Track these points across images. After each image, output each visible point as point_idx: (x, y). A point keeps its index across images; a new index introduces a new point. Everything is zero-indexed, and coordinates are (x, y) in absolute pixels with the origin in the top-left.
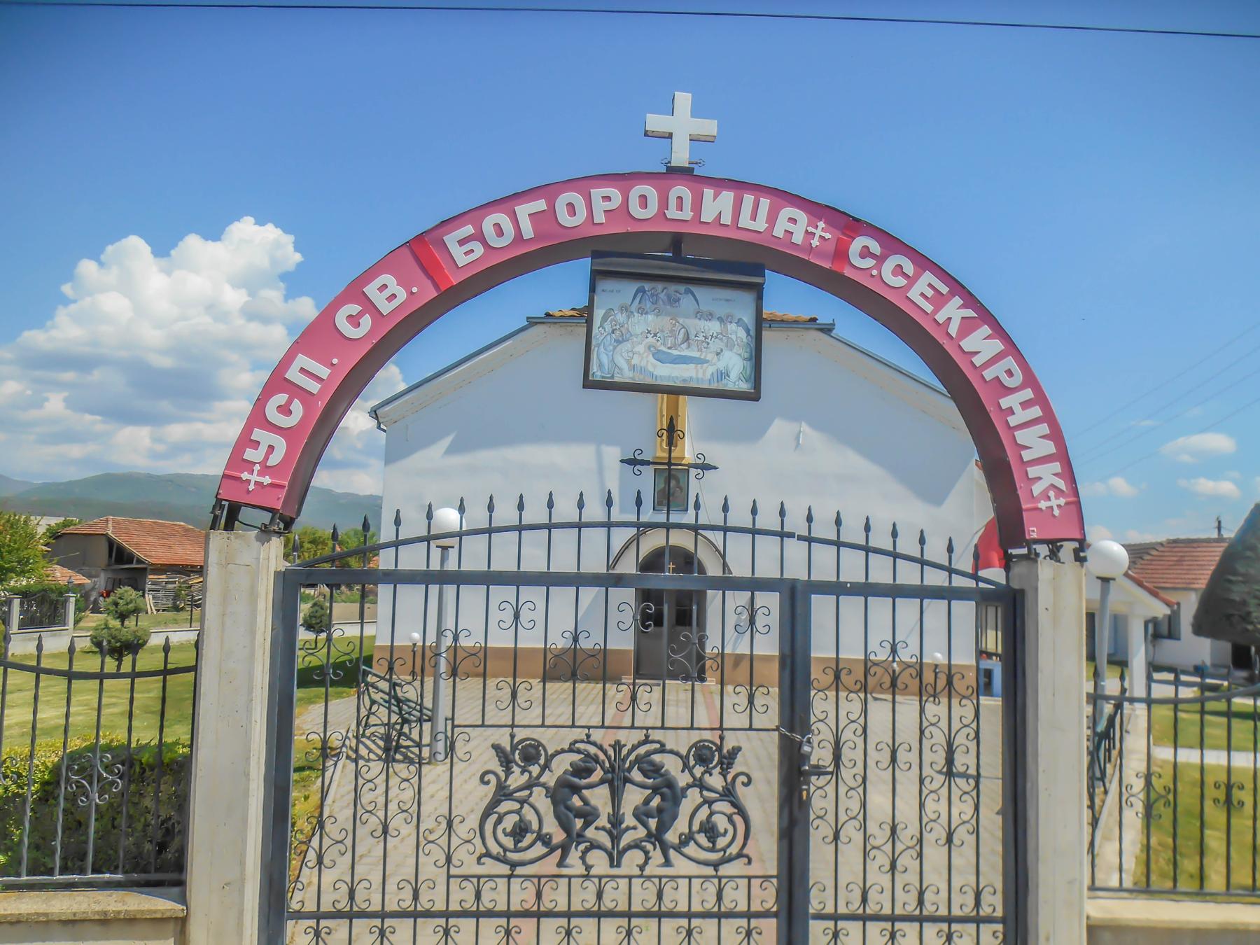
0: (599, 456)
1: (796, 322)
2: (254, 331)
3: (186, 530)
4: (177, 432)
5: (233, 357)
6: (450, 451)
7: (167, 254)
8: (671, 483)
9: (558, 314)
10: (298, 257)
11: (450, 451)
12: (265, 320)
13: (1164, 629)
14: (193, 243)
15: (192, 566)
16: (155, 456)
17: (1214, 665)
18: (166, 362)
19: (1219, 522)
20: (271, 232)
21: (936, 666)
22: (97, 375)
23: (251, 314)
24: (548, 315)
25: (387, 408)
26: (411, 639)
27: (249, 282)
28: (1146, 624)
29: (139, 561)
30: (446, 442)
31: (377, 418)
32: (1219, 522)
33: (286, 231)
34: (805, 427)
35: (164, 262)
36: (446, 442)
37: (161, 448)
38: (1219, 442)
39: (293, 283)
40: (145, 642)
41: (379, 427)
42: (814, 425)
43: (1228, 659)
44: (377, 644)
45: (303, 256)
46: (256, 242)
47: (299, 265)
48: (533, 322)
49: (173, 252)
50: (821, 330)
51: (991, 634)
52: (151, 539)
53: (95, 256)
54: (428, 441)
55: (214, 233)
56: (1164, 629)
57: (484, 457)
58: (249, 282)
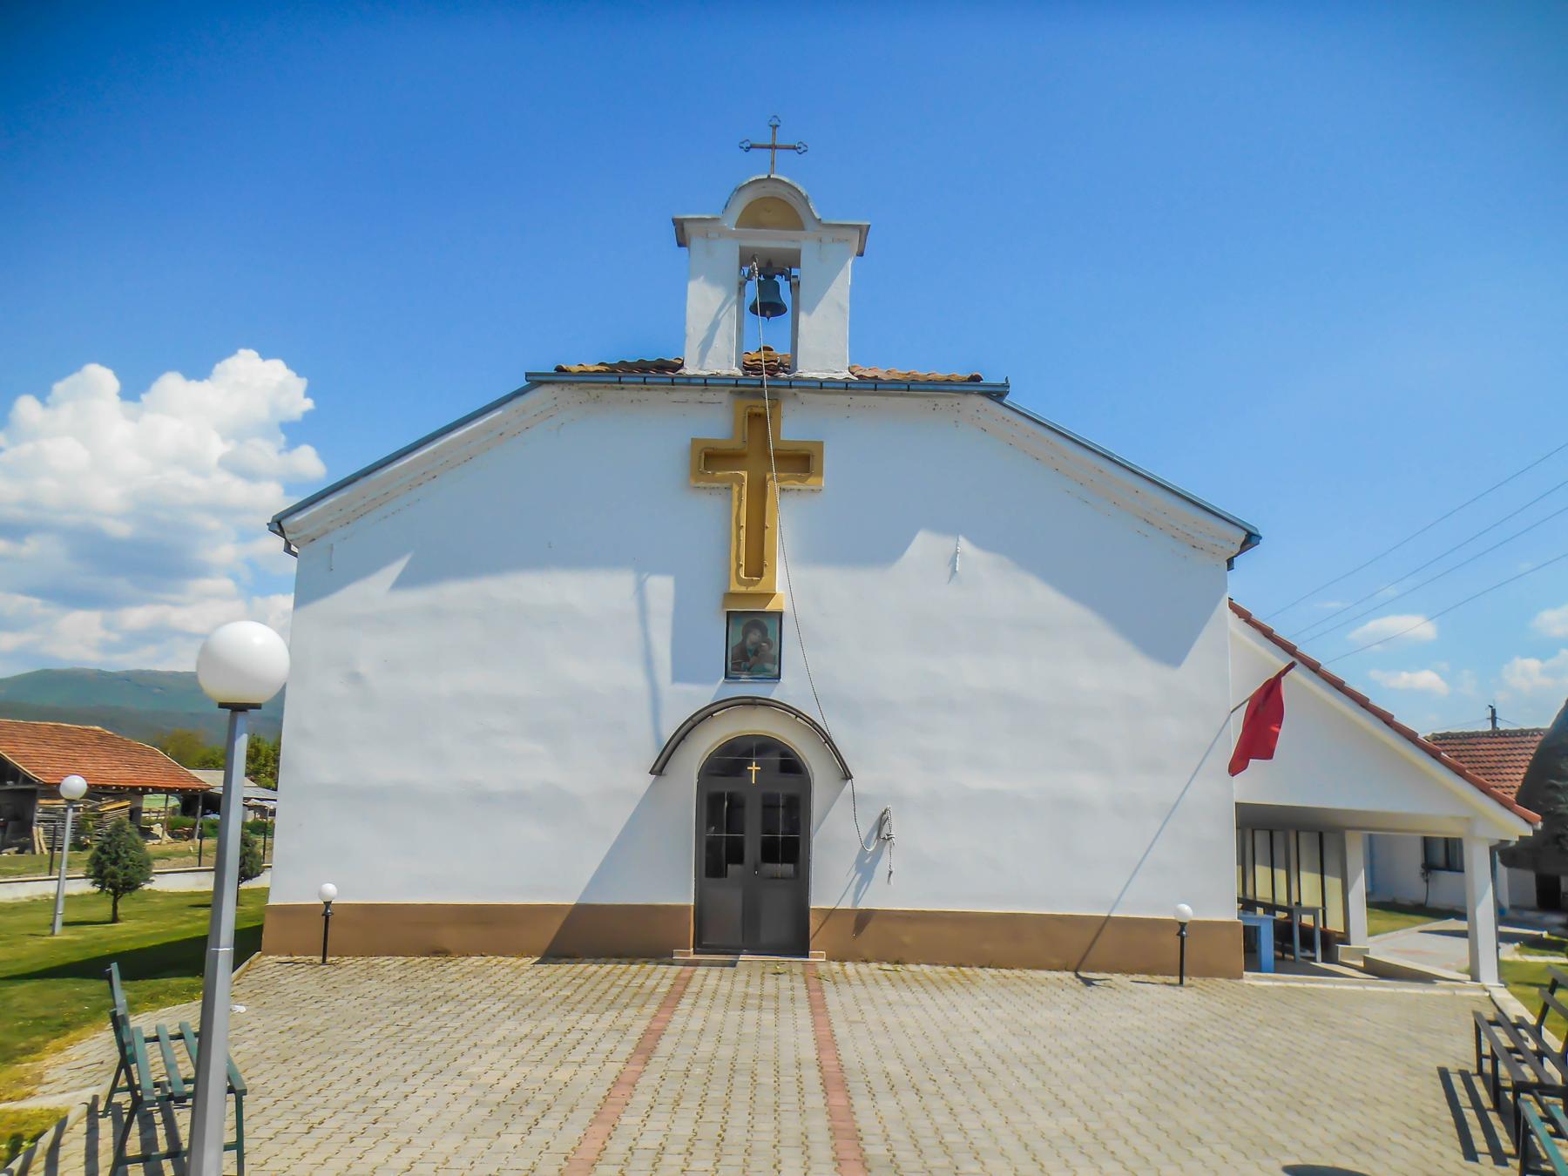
0: (640, 588)
1: (948, 381)
2: (238, 491)
3: (102, 737)
4: (137, 617)
5: (213, 524)
6: (402, 582)
7: (136, 399)
8: (753, 642)
9: (575, 368)
10: (309, 404)
11: (402, 582)
12: (249, 475)
13: (1439, 856)
14: (172, 385)
15: (105, 787)
16: (107, 648)
17: (1513, 907)
18: (121, 530)
19: (1494, 712)
20: (276, 371)
21: (1183, 925)
22: (31, 547)
23: (226, 464)
24: (560, 369)
25: (298, 518)
26: (321, 894)
27: (236, 433)
28: (1492, 850)
29: (28, 780)
30: (396, 569)
31: (282, 533)
32: (1494, 712)
33: (299, 375)
34: (964, 545)
35: (131, 405)
36: (396, 569)
37: (115, 637)
38: (1416, 626)
39: (294, 432)
40: (137, 887)
41: (288, 549)
42: (976, 542)
43: (1532, 897)
44: (271, 903)
45: (316, 403)
46: (258, 383)
47: (307, 415)
48: (535, 381)
49: (143, 397)
50: (988, 395)
51: (1262, 872)
52: (47, 749)
53: (42, 394)
54: (366, 568)
55: (198, 369)
56: (1439, 856)
57: (455, 592)
58: (236, 433)
